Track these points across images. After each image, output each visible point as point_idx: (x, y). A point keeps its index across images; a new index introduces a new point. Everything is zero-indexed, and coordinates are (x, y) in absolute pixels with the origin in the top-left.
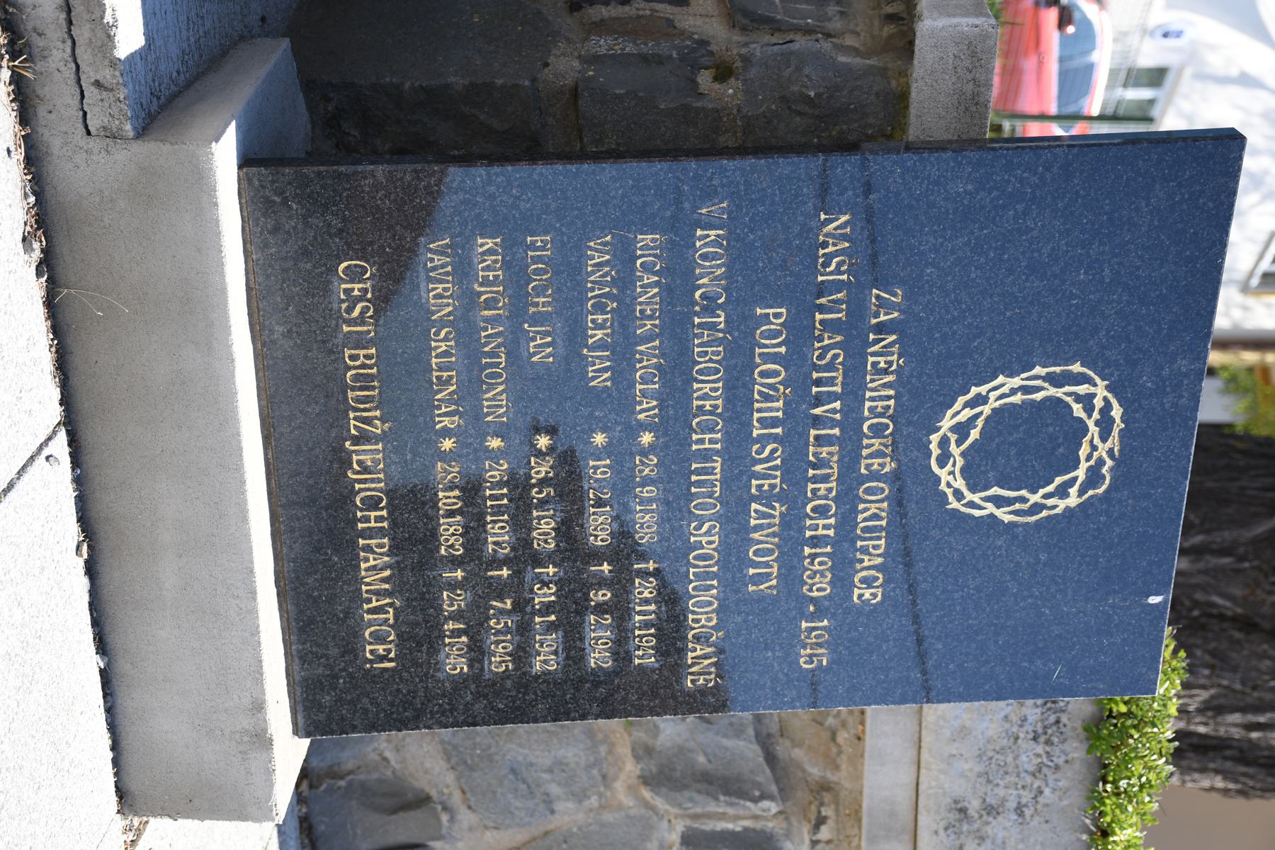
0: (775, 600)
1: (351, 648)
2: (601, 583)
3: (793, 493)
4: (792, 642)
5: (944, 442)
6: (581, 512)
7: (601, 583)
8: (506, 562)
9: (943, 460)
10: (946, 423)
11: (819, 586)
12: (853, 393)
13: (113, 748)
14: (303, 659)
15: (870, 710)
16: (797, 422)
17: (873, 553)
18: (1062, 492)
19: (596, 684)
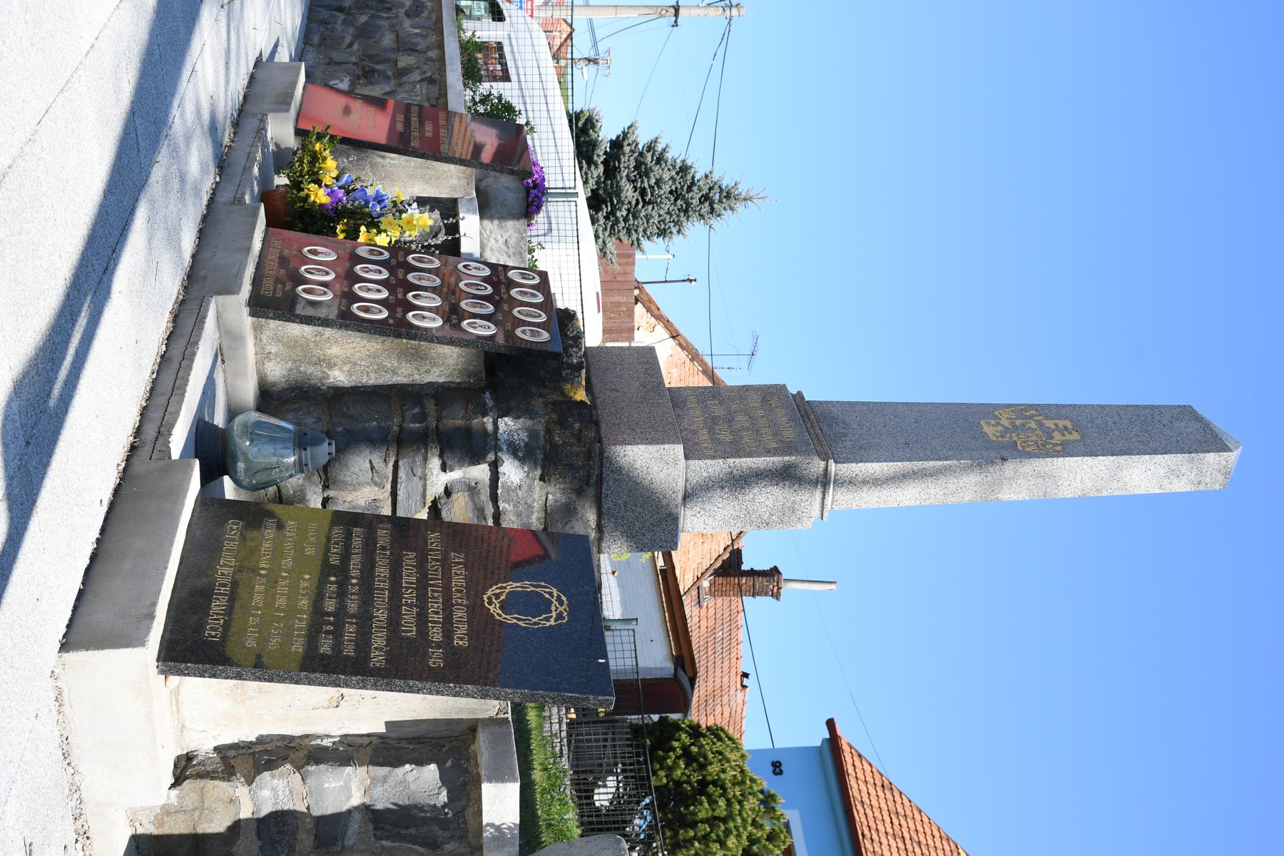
0: (415, 640)
1: (200, 627)
2: (329, 623)
3: (422, 599)
4: (425, 656)
5: (489, 598)
6: (322, 599)
7: (329, 623)
8: (283, 611)
9: (490, 603)
10: (489, 593)
11: (436, 635)
12: (447, 578)
13: (68, 626)
14: (172, 632)
15: (485, 822)
16: (422, 584)
17: (461, 630)
18: (547, 619)
19: (323, 660)
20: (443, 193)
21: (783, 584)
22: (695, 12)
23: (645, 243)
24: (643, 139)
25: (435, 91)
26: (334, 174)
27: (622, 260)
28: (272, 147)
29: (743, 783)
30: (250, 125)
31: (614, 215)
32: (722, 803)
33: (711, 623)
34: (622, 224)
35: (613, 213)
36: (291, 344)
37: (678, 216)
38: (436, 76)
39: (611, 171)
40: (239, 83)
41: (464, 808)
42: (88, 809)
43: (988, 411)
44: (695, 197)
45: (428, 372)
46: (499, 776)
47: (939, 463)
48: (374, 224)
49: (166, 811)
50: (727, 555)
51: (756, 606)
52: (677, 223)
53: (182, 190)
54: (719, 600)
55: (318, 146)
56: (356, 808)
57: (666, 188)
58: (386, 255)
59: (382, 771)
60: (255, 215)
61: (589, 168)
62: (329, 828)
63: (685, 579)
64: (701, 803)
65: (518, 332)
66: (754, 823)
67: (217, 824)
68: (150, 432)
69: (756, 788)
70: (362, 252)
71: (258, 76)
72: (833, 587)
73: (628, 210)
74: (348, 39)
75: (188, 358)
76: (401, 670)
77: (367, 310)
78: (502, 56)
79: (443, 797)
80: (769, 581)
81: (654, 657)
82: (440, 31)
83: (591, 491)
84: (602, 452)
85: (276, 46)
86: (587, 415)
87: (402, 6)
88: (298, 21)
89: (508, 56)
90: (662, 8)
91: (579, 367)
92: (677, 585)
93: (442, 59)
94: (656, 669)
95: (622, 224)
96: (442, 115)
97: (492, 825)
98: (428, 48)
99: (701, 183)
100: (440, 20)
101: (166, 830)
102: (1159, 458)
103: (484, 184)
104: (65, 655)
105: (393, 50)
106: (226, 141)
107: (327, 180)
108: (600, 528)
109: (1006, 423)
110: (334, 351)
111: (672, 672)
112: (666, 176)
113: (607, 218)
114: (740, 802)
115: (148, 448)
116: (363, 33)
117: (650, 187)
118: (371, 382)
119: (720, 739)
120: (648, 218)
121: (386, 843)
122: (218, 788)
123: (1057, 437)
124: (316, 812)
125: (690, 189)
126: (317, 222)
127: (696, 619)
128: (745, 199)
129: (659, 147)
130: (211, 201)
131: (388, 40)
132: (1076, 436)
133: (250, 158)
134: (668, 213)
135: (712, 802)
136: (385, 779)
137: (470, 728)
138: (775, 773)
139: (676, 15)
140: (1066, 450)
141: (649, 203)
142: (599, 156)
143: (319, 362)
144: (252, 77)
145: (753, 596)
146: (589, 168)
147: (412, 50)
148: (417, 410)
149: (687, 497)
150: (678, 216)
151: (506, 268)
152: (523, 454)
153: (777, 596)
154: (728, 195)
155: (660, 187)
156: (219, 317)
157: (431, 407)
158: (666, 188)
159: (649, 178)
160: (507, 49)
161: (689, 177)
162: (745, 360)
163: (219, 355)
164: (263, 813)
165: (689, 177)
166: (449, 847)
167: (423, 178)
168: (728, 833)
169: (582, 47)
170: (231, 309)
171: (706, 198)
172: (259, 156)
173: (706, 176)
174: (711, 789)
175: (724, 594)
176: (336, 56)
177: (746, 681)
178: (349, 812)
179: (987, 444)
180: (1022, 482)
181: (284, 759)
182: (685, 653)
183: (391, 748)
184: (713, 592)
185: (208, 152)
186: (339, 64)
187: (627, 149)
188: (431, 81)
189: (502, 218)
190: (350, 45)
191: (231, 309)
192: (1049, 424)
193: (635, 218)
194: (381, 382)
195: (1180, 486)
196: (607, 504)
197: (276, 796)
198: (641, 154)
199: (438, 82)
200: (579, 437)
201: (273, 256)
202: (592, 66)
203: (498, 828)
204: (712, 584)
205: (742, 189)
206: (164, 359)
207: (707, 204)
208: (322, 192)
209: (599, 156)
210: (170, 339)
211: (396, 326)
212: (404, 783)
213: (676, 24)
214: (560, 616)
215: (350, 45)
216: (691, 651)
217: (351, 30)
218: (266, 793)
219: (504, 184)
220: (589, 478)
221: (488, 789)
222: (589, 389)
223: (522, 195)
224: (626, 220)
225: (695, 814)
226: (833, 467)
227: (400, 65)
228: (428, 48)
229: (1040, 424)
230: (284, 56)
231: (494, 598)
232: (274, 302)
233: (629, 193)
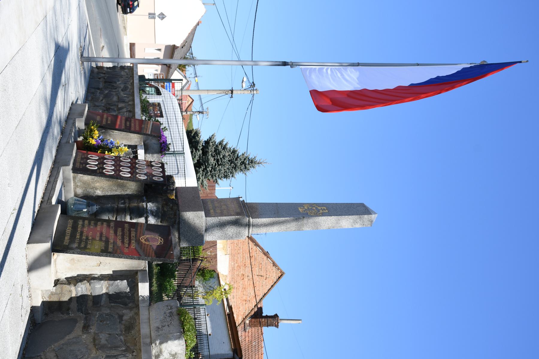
20: (132, 143)
21: (279, 321)
22: (239, 92)
23: (219, 181)
24: (218, 140)
25: (131, 114)
26: (98, 135)
27: (211, 188)
28: (77, 129)
30: (71, 121)
31: (206, 170)
33: (250, 339)
34: (209, 173)
35: (206, 169)
36: (84, 183)
38: (132, 110)
39: (205, 152)
40: (67, 110)
41: (134, 293)
42: (32, 290)
43: (301, 205)
44: (239, 162)
45: (126, 191)
46: (143, 281)
47: (284, 219)
48: (110, 150)
49: (52, 294)
50: (256, 309)
51: (267, 331)
52: (231, 173)
53: (53, 139)
54: (253, 329)
55: (92, 127)
56: (104, 294)
57: (227, 159)
58: (114, 158)
59: (111, 282)
60: (74, 146)
61: (196, 151)
62: (97, 299)
63: (238, 319)
65: (154, 178)
67: (66, 298)
68: (46, 198)
70: (106, 157)
71: (73, 107)
72: (300, 322)
73: (212, 168)
74: (101, 98)
75: (53, 189)
77: (108, 172)
78: (160, 108)
79: (128, 290)
80: (273, 320)
82: (133, 95)
83: (176, 226)
84: (179, 214)
85: (77, 99)
86: (175, 203)
87: (121, 87)
88: (84, 92)
89: (163, 108)
90: (226, 91)
91: (173, 190)
92: (235, 323)
93: (134, 105)
94: (225, 354)
95: (209, 173)
96: (133, 120)
97: (141, 296)
98: (129, 101)
100: (133, 92)
101: (52, 300)
102: (350, 217)
103: (146, 142)
104: (31, 245)
105: (117, 102)
106: (64, 126)
107: (95, 137)
108: (179, 238)
109: (306, 208)
110: (97, 185)
111: (232, 355)
112: (227, 154)
113: (203, 171)
115: (46, 202)
116: (106, 96)
117: (221, 159)
118: (109, 194)
120: (220, 170)
121: (112, 304)
122: (66, 287)
123: (321, 211)
124: (93, 294)
125: (236, 159)
126: (94, 149)
127: (244, 337)
128: (259, 163)
129: (224, 143)
130: (60, 142)
131: (115, 99)
132: (327, 211)
133: (71, 131)
134: (228, 169)
136: (112, 285)
139: (232, 93)
140: (323, 215)
141: (220, 165)
142: (200, 147)
143: (93, 188)
144: (71, 108)
145: (267, 326)
146: (196, 151)
147: (124, 102)
148: (123, 201)
149: (206, 230)
151: (151, 162)
152: (155, 214)
153: (277, 326)
154: (252, 162)
155: (224, 159)
156: (63, 173)
157: (127, 201)
158: (227, 159)
159: (220, 155)
160: (162, 105)
161: (236, 155)
163: (63, 184)
164: (79, 295)
165: (236, 155)
166: (130, 305)
167: (126, 139)
169: (196, 107)
170: (67, 171)
171: (243, 163)
172: (74, 130)
173: (243, 154)
175: (255, 326)
176: (97, 104)
178: (102, 294)
179: (299, 213)
180: (309, 225)
181: (85, 280)
182: (238, 348)
183: (116, 276)
184: (251, 325)
185: (59, 130)
186: (98, 106)
187: (211, 144)
188: (130, 111)
189: (153, 153)
190: (102, 100)
191: (67, 171)
192: (319, 208)
193: (215, 171)
194: (112, 194)
195: (358, 226)
196: (181, 231)
197: (82, 290)
198: (217, 146)
199: (133, 112)
200: (172, 209)
201: (79, 160)
202: (201, 115)
203: (143, 297)
204: (250, 322)
205: (257, 159)
206: (49, 182)
207: (243, 165)
208: (93, 140)
209: (200, 147)
210: (50, 177)
211: (117, 176)
212: (117, 285)
213: (232, 97)
214: (161, 243)
215: (102, 100)
217: (102, 95)
218: (79, 289)
219: (153, 142)
220: (175, 221)
221: (140, 285)
222: (176, 196)
223: (159, 146)
224: (211, 172)
226: (251, 220)
227: (119, 106)
228: (129, 101)
229: (316, 208)
230: (79, 102)
232: (80, 168)
233: (212, 161)
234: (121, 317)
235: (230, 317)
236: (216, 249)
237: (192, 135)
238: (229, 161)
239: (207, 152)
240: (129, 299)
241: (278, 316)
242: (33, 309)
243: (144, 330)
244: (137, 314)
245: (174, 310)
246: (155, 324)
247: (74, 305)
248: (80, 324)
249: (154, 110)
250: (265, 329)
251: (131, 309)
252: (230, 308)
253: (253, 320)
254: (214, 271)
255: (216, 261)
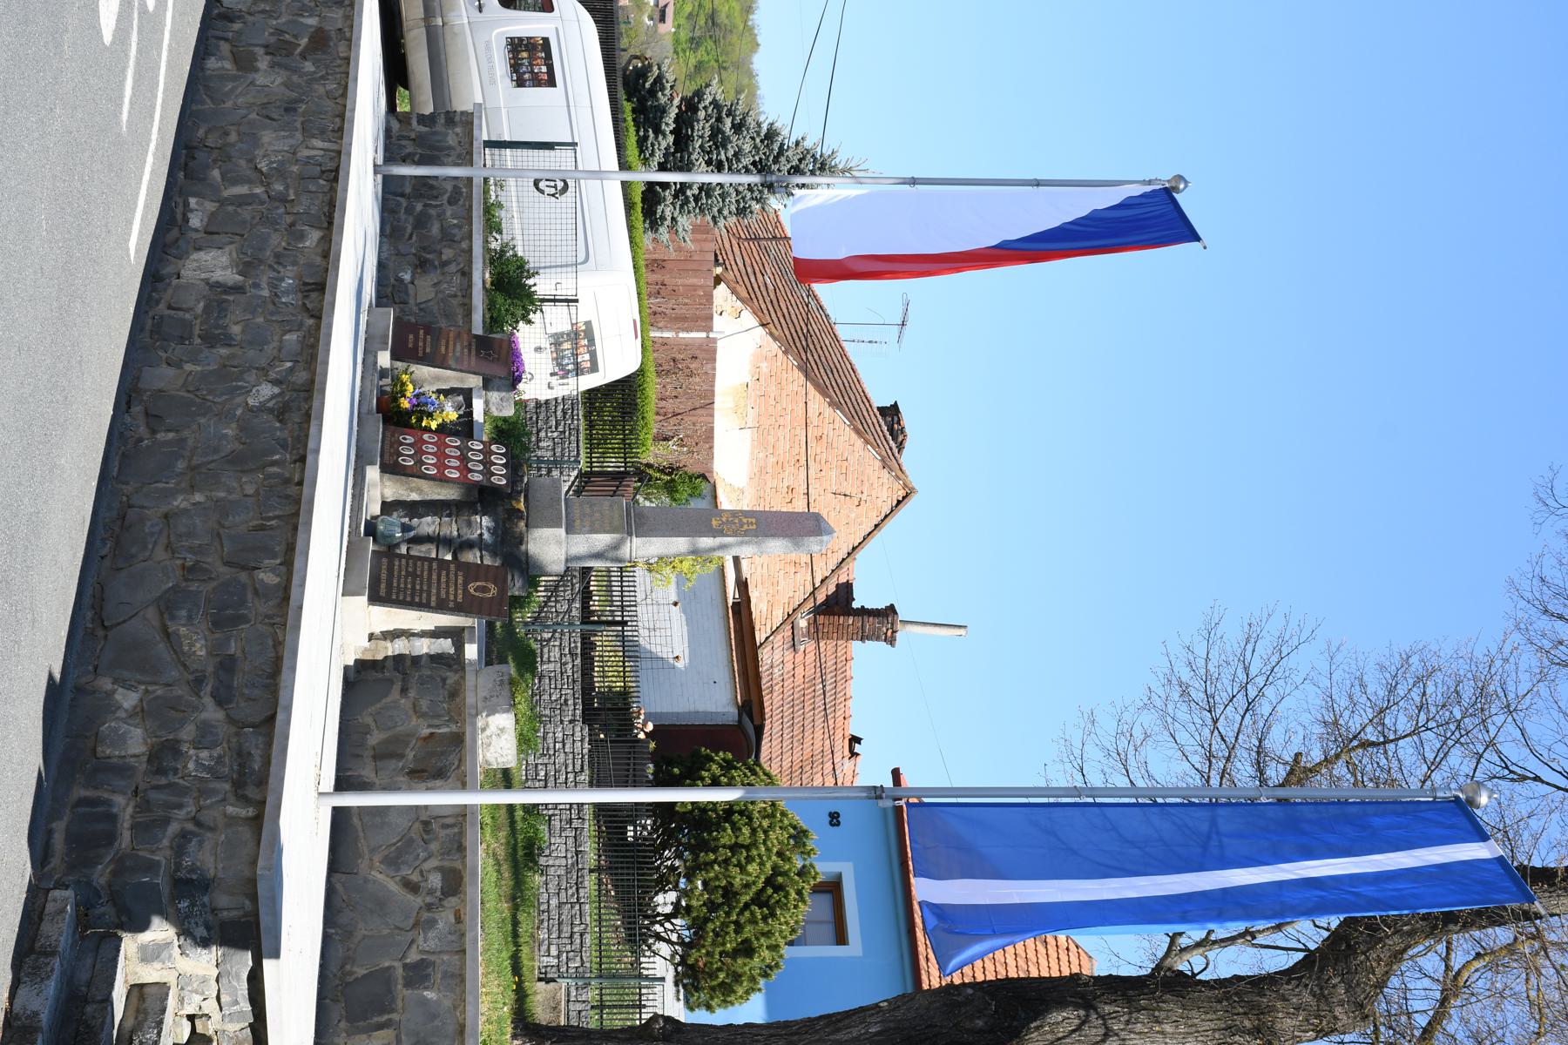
16: (447, 582)
21: (899, 626)
29: (773, 816)
31: (684, 193)
32: (746, 831)
33: (810, 672)
37: (761, 192)
46: (471, 642)
51: (864, 655)
52: (758, 201)
62: (416, 660)
63: (766, 612)
64: (725, 830)
66: (779, 854)
67: (380, 657)
69: (786, 822)
72: (962, 631)
76: (441, 607)
78: (549, 57)
79: (452, 651)
80: (881, 624)
81: (715, 699)
99: (790, 153)
112: (747, 148)
114: (765, 832)
119: (754, 773)
131: (435, 230)
135: (736, 829)
137: (463, 629)
138: (832, 824)
150: (761, 192)
153: (891, 641)
155: (738, 161)
162: (896, 329)
165: (776, 147)
168: (749, 859)
173: (797, 143)
174: (736, 817)
177: (857, 748)
183: (437, 633)
190: (411, 237)
193: (708, 196)
205: (840, 161)
216: (760, 690)
225: (716, 839)
227: (444, 257)
231: (471, 588)
234: (444, 680)
235: (741, 611)
236: (712, 416)
237: (647, 85)
238: (754, 164)
239: (690, 138)
240: (454, 662)
241: (895, 612)
242: (346, 668)
243: (470, 699)
244: (463, 678)
245: (506, 678)
246: (482, 693)
247: (390, 664)
248: (397, 687)
249: (531, 65)
250: (856, 645)
251: (456, 671)
252: (742, 585)
253: (821, 619)
254: (704, 477)
255: (711, 448)
